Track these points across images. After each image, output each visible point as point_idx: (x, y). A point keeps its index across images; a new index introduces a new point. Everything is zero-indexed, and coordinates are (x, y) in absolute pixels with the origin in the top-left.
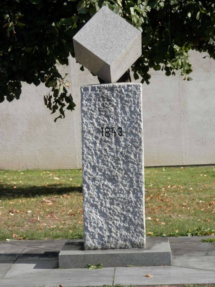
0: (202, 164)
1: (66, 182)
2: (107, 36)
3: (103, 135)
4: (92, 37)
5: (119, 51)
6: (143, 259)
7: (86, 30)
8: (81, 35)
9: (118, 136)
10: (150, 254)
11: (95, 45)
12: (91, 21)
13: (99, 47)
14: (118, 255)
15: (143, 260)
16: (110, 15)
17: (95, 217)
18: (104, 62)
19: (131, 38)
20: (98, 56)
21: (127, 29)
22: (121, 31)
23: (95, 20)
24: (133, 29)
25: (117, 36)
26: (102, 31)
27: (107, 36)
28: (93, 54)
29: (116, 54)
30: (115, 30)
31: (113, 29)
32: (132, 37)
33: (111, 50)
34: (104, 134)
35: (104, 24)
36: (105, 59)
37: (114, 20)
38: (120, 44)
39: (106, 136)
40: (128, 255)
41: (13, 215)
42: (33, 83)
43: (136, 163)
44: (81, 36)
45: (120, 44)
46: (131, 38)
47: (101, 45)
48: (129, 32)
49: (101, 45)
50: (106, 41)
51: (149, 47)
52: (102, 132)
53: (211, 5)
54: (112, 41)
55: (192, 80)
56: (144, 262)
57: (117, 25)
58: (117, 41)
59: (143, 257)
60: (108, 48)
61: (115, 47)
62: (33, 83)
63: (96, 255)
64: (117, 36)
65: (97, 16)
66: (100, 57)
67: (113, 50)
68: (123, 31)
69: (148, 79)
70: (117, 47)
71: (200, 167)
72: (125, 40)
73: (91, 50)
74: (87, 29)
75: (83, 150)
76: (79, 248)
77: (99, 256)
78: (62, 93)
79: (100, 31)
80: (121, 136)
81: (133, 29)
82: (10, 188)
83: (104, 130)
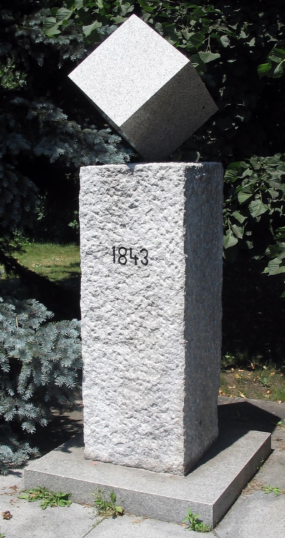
0: (238, 501)
4: (101, 73)
6: (161, 507)
7: (93, 60)
8: (83, 71)
12: (106, 44)
16: (140, 30)
21: (164, 56)
25: (143, 69)
26: (119, 62)
36: (113, 114)
42: (68, 76)
44: (81, 72)
46: (169, 73)
47: (112, 87)
48: (168, 60)
49: (112, 87)
58: (143, 79)
62: (68, 76)
69: (257, 69)
71: (233, 499)
72: (157, 77)
82: (5, 236)
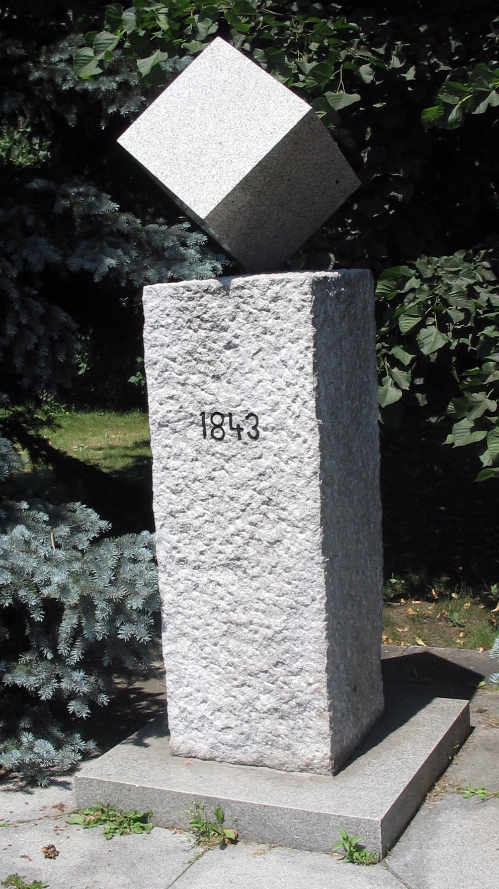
1: (301, 623)
2: (211, 127)
3: (205, 435)
5: (237, 172)
6: (297, 827)
7: (156, 113)
8: (140, 132)
10: (317, 817)
11: (173, 158)
13: (183, 163)
15: (299, 830)
19: (278, 129)
21: (271, 102)
22: (254, 110)
23: (186, 82)
24: (288, 100)
26: (198, 114)
29: (227, 183)
30: (237, 106)
32: (282, 126)
33: (214, 172)
34: (208, 432)
35: (210, 90)
36: (192, 199)
37: (238, 76)
38: (243, 150)
39: (213, 437)
41: (439, 645)
43: (300, 525)
44: (138, 133)
45: (243, 150)
46: (280, 129)
50: (206, 143)
52: (204, 425)
54: (220, 143)
55: (335, 774)
56: (300, 836)
57: (243, 92)
58: (237, 140)
59: (298, 821)
60: (207, 163)
64: (238, 125)
65: (192, 69)
67: (220, 168)
68: (258, 108)
70: (233, 161)
74: (159, 111)
77: (175, 797)
79: (192, 115)
80: (256, 438)
81: (288, 100)
83: (208, 421)
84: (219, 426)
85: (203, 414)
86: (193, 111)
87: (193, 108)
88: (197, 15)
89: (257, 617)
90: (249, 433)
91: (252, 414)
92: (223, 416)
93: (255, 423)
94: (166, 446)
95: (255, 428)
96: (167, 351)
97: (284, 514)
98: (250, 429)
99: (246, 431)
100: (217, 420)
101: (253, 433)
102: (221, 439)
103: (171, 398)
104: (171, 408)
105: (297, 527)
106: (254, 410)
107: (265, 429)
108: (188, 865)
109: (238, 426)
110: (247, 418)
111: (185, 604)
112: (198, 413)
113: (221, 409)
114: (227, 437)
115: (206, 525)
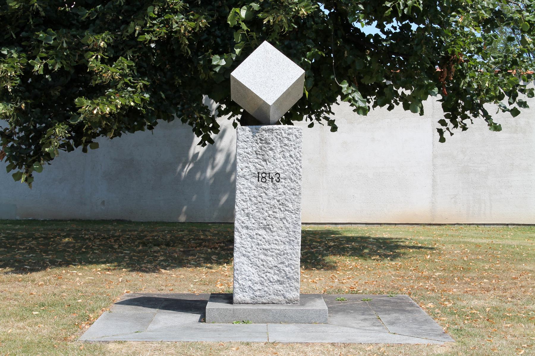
2: (268, 74)
3: (258, 181)
9: (275, 182)
14: (270, 310)
17: (246, 269)
18: (264, 101)
20: (258, 94)
27: (268, 74)
28: (253, 92)
31: (275, 67)
33: (272, 89)
34: (260, 180)
38: (282, 83)
39: (262, 181)
40: (281, 310)
43: (293, 212)
51: (50, 80)
52: (259, 177)
53: (200, 60)
61: (276, 85)
63: (247, 310)
66: (260, 96)
71: (384, 226)
73: (250, 89)
75: (374, 259)
76: (226, 301)
78: (168, 122)
80: (278, 182)
83: (260, 175)
84: (265, 177)
85: (258, 173)
86: (260, 67)
87: (260, 66)
88: (465, 28)
89: (273, 246)
90: (276, 180)
91: (277, 173)
92: (266, 174)
93: (278, 176)
94: (243, 184)
95: (278, 178)
96: (246, 150)
97: (287, 208)
98: (276, 178)
99: (275, 179)
100: (264, 175)
101: (278, 180)
102: (265, 182)
103: (246, 167)
104: (246, 171)
105: (292, 213)
106: (278, 172)
107: (282, 179)
108: (296, 346)
109: (272, 177)
110: (276, 175)
111: (245, 243)
112: (257, 173)
113: (267, 171)
114: (267, 181)
115: (257, 213)
